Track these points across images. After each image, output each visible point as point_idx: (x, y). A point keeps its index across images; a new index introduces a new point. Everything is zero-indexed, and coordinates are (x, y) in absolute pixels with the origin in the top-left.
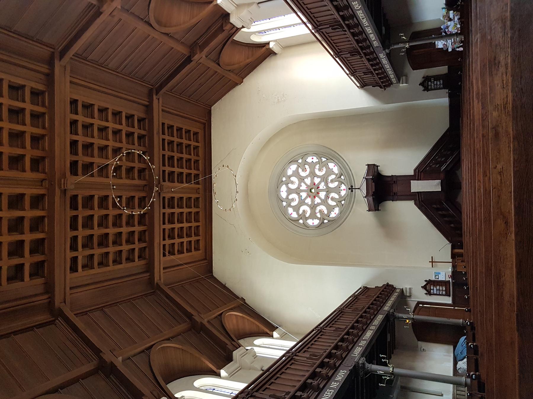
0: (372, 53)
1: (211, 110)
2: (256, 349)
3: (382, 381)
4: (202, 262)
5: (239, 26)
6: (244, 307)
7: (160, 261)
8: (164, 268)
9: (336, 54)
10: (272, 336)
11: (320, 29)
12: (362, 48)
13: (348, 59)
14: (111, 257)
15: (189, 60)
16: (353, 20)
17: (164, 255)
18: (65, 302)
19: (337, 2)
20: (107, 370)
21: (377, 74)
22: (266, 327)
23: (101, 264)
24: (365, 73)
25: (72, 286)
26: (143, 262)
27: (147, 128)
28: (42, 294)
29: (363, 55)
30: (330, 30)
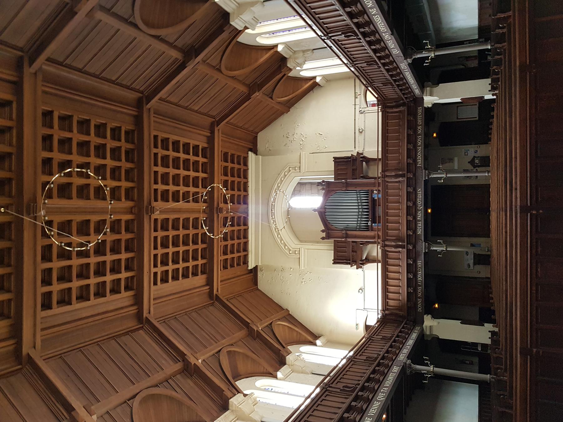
0: (391, 63)
1: (257, 136)
2: (304, 356)
3: (425, 379)
4: (245, 276)
5: (240, 29)
6: (289, 318)
7: (151, 291)
8: (221, 281)
9: (351, 63)
10: (275, 377)
11: (331, 37)
12: (358, 25)
13: (365, 68)
14: (92, 290)
15: (248, 98)
16: (356, 7)
17: (155, 283)
18: (35, 348)
19: (351, 8)
20: (189, 370)
21: (398, 86)
22: (310, 337)
23: (61, 302)
24: (384, 84)
25: (155, 297)
26: (130, 293)
27: (136, 141)
28: (132, 305)
29: (380, 65)
30: (342, 37)
